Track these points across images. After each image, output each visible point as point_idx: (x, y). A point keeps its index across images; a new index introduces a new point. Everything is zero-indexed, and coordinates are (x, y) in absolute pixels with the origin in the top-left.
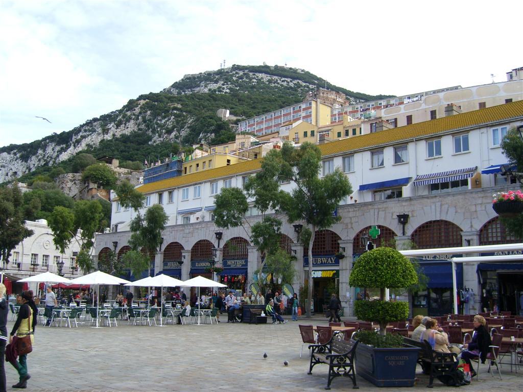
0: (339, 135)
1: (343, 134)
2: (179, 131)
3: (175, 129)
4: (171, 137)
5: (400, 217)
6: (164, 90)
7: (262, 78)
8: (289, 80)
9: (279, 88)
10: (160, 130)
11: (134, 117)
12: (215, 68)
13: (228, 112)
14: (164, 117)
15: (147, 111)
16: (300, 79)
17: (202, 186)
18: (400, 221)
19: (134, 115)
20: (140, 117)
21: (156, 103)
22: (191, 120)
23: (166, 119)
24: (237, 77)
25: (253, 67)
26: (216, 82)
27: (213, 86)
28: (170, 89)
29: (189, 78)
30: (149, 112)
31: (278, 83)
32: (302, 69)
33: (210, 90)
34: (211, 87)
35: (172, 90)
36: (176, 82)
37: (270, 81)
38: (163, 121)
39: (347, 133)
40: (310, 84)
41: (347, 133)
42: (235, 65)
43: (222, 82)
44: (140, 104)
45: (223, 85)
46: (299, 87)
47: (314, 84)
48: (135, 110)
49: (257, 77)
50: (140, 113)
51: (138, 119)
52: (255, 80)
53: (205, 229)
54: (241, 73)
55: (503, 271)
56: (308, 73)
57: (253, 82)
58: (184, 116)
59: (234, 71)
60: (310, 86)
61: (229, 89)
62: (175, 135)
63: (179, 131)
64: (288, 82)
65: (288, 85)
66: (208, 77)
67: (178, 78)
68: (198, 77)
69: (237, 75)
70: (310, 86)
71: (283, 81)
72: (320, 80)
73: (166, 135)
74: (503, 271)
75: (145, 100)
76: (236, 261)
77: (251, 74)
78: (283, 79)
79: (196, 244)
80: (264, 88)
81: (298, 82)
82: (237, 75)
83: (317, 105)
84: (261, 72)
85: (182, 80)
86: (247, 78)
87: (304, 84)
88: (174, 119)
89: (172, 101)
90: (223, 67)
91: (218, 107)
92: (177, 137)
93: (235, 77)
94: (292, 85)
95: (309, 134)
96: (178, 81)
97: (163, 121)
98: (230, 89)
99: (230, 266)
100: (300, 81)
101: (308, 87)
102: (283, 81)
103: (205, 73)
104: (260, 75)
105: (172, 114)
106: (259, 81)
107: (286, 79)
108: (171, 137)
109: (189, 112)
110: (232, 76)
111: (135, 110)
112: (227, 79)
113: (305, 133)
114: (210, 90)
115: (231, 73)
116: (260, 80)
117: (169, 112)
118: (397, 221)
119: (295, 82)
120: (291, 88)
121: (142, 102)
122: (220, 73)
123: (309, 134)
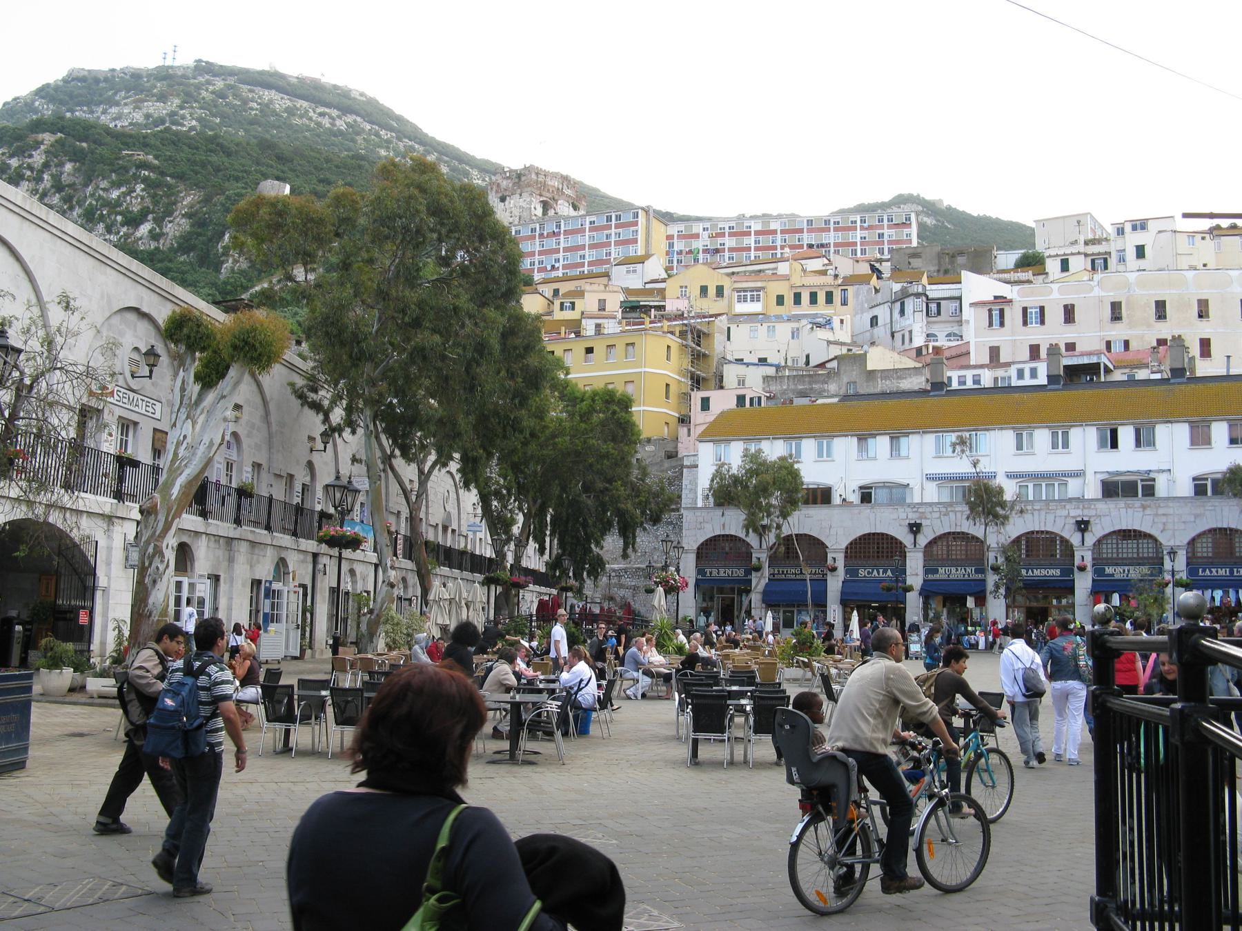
0: (780, 300)
1: (789, 299)
2: (159, 221)
3: (150, 217)
4: (138, 234)
5: (1079, 523)
6: (15, 99)
7: (271, 101)
8: (335, 113)
9: (313, 130)
10: (109, 215)
11: (29, 173)
12: (147, 60)
13: (288, 187)
14: (117, 185)
15: (61, 164)
16: (358, 115)
17: (733, 443)
18: (911, 531)
19: (30, 168)
20: (46, 176)
21: (84, 145)
22: (189, 199)
23: (123, 189)
24: (213, 93)
25: (247, 71)
26: (162, 98)
27: (156, 109)
28: (33, 101)
29: (83, 79)
30: (68, 167)
31: (310, 119)
32: (361, 90)
33: (147, 116)
34: (151, 111)
35: (37, 103)
36: (48, 85)
37: (291, 111)
38: (115, 194)
39: (797, 299)
40: (382, 127)
41: (797, 299)
42: (200, 61)
43: (177, 101)
44: (42, 143)
45: (182, 108)
46: (358, 134)
47: (391, 129)
48: (31, 156)
49: (260, 97)
50: (46, 165)
51: (39, 179)
52: (255, 105)
53: (1043, 513)
54: (219, 84)
55: (1044, 572)
56: (372, 102)
57: (252, 109)
58: (169, 187)
59: (201, 75)
60: (382, 133)
61: (198, 120)
62: (150, 231)
63: (159, 221)
64: (333, 119)
65: (333, 125)
66: (134, 83)
67: (54, 74)
68: (106, 80)
69: (211, 88)
70: (382, 133)
71: (322, 115)
72: (399, 119)
73: (125, 229)
74: (1044, 572)
75: (53, 133)
76: (1126, 568)
77: (245, 87)
78: (321, 109)
79: (860, 538)
80: (279, 127)
81: (355, 121)
82: (211, 88)
83: (648, 220)
84: (268, 86)
85: (65, 81)
86: (236, 96)
87: (368, 127)
88: (143, 190)
89: (127, 146)
90: (169, 63)
91: (266, 177)
92: (154, 236)
93: (207, 90)
94: (341, 125)
95: (712, 291)
96: (51, 81)
97: (115, 194)
98: (199, 120)
99: (1113, 575)
100: (359, 119)
101: (377, 135)
102: (321, 114)
103: (123, 71)
104: (267, 95)
105: (136, 178)
106: (266, 108)
107: (327, 110)
108: (138, 234)
109: (180, 177)
110: (198, 87)
111: (31, 156)
112: (188, 94)
113: (704, 290)
114: (147, 116)
115: (192, 81)
116: (267, 106)
117: (127, 172)
118: (1073, 527)
119: (350, 119)
120: (341, 133)
121: (48, 138)
122: (165, 75)
123: (712, 291)
